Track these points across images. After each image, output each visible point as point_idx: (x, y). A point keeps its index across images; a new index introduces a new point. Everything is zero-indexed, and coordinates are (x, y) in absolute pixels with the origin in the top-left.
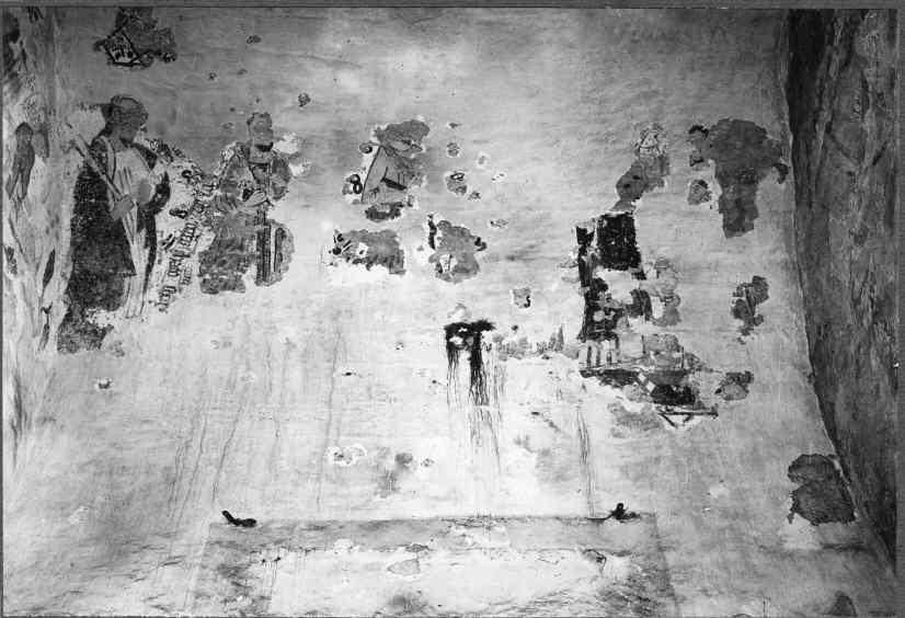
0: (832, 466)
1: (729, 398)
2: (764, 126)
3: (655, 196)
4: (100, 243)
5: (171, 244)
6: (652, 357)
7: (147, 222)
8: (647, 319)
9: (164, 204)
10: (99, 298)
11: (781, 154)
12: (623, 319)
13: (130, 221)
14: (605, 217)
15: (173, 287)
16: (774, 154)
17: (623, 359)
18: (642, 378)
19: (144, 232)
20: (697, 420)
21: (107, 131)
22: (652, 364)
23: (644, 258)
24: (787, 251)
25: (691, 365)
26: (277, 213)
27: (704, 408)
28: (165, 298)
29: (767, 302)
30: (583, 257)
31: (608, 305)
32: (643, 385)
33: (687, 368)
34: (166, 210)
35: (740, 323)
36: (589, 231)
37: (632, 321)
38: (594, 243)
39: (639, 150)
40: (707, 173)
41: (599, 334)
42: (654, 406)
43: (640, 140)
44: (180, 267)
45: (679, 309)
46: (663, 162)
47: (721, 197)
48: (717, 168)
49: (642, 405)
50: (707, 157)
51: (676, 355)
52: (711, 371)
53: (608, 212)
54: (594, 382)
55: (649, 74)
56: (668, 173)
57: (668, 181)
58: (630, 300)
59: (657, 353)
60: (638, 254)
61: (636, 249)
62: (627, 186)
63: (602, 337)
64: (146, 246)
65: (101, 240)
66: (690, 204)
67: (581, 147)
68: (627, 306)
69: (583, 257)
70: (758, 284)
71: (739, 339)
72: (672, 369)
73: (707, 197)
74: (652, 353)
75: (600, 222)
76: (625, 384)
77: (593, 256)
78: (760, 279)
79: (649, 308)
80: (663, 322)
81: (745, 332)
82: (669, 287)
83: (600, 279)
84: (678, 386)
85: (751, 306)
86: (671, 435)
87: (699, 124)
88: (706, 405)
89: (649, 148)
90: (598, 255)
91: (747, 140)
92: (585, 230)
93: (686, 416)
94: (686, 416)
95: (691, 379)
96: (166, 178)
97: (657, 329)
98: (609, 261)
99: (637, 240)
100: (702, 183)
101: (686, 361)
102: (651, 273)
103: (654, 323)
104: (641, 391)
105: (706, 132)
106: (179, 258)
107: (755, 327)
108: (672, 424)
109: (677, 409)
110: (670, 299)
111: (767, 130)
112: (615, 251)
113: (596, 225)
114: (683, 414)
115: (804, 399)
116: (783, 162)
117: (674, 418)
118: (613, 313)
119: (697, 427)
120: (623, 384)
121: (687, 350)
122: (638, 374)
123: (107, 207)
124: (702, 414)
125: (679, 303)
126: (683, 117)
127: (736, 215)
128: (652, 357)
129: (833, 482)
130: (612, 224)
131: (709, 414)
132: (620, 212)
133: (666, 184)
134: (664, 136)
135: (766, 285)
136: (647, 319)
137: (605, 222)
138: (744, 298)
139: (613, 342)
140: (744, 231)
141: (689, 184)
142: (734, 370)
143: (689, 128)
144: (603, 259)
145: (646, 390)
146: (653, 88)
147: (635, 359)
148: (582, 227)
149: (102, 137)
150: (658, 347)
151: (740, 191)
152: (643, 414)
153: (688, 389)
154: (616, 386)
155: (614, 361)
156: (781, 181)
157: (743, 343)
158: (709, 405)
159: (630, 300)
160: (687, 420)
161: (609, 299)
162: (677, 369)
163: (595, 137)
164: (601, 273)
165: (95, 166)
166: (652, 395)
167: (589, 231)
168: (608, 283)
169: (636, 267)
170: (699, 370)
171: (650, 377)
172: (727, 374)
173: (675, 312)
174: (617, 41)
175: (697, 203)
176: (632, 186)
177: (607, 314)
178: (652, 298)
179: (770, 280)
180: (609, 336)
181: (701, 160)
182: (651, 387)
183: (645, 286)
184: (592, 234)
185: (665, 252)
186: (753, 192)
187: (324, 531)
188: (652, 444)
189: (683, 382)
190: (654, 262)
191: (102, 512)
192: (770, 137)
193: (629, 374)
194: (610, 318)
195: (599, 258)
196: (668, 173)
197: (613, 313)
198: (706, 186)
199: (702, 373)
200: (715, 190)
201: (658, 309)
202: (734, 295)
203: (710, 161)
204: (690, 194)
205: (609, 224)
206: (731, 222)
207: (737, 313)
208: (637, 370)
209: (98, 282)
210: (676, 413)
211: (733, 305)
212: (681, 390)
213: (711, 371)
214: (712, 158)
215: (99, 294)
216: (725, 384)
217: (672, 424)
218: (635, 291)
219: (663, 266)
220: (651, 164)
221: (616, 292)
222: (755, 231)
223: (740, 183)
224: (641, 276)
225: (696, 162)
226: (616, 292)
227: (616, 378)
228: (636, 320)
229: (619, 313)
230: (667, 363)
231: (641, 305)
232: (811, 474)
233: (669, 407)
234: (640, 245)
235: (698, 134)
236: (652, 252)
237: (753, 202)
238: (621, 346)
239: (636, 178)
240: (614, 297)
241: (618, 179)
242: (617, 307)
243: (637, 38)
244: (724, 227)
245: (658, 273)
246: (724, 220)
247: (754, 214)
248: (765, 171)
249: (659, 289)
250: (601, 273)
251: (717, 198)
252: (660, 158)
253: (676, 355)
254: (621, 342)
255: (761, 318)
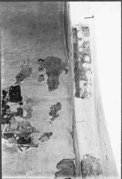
0: (73, 163)
1: (43, 141)
2: (61, 58)
3: (27, 80)
6: (20, 129)
8: (21, 117)
11: (66, 66)
12: (13, 117)
14: (12, 87)
16: (64, 66)
17: (11, 130)
18: (15, 135)
20: (30, 148)
22: (20, 131)
23: (23, 98)
24: (68, 95)
25: (33, 131)
26: (6, 105)
27: (34, 145)
29: (60, 111)
30: (4, 99)
31: (9, 113)
32: (15, 138)
33: (31, 132)
35: (51, 117)
36: (6, 91)
37: (15, 117)
38: (8, 95)
39: (23, 67)
40: (44, 72)
41: (5, 122)
42: (17, 144)
43: (23, 64)
45: (32, 113)
46: (30, 69)
47: (48, 79)
48: (47, 71)
49: (13, 144)
50: (44, 68)
51: (28, 128)
52: (39, 132)
53: (13, 85)
55: (25, 45)
56: (32, 73)
57: (32, 75)
58: (16, 111)
59: (22, 127)
60: (22, 98)
61: (21, 96)
62: (19, 77)
63: (5, 123)
66: (38, 82)
67: (6, 66)
68: (15, 113)
69: (4, 99)
70: (58, 105)
71: (50, 122)
72: (26, 132)
73: (44, 79)
74: (21, 127)
75: (10, 88)
76: (9, 138)
77: (7, 98)
78: (59, 103)
79: (22, 113)
80: (26, 118)
81: (52, 120)
82: (30, 107)
83: (8, 106)
84: (26, 138)
85: (55, 111)
86: (20, 154)
87: (41, 58)
88: (35, 144)
89: (26, 66)
90: (9, 98)
91: (56, 62)
92: (5, 91)
93: (27, 148)
94: (27, 148)
95: (32, 135)
97: (24, 120)
98: (12, 100)
99: (21, 93)
100: (42, 76)
101: (31, 129)
102: (25, 103)
103: (23, 118)
104: (14, 140)
105: (43, 61)
107: (56, 118)
108: (21, 150)
109: (25, 145)
110: (29, 111)
111: (62, 59)
112: (14, 97)
113: (9, 89)
114: (26, 147)
115: (68, 140)
116: (67, 68)
117: (22, 148)
118: (10, 115)
119: (30, 150)
120: (8, 138)
121: (32, 126)
122: (14, 134)
124: (32, 147)
125: (32, 111)
126: (37, 57)
127: (52, 84)
128: (20, 129)
129: (72, 168)
130: (14, 89)
131: (35, 146)
132: (17, 85)
133: (31, 76)
134: (31, 62)
135: (61, 105)
136: (21, 117)
137: (12, 88)
138: (54, 109)
139: (9, 124)
140: (55, 89)
141: (38, 76)
142: (47, 132)
143: (38, 60)
144: (10, 100)
145: (16, 139)
146: (27, 48)
147: (14, 130)
148: (4, 90)
150: (23, 125)
151: (54, 77)
152: (12, 147)
153: (30, 139)
154: (6, 139)
155: (7, 130)
156: (66, 73)
157: (51, 123)
158: (35, 144)
159: (16, 111)
160: (27, 149)
161: (10, 111)
162: (28, 132)
163: (10, 64)
164: (9, 104)
166: (17, 141)
167: (6, 91)
168: (10, 106)
169: (21, 101)
170: (35, 132)
171: (18, 135)
172: (44, 133)
173: (30, 114)
174: (15, 35)
175: (41, 81)
176: (20, 77)
177: (8, 116)
178: (24, 110)
179: (62, 103)
180: (7, 122)
181: (42, 69)
182: (18, 138)
183: (22, 107)
184: (7, 92)
185: (30, 96)
186: (58, 77)
188: (12, 157)
189: (29, 137)
190: (26, 100)
192: (62, 61)
193: (11, 134)
194: (9, 117)
195: (9, 99)
196: (32, 73)
197: (10, 115)
198: (43, 76)
199: (36, 133)
200: (46, 77)
201: (25, 113)
202: (50, 108)
203: (44, 69)
204: (38, 79)
205: (13, 89)
206: (51, 87)
207: (51, 114)
208: (14, 133)
210: (24, 147)
211: (50, 112)
212: (28, 139)
213: (39, 132)
214: (45, 68)
216: (43, 136)
217: (21, 150)
218: (18, 108)
219: (29, 101)
220: (26, 70)
221: (12, 109)
222: (58, 89)
223: (54, 75)
224: (21, 104)
225: (40, 69)
226: (12, 109)
227: (7, 136)
228: (18, 117)
229: (12, 115)
230: (25, 130)
231: (20, 113)
232: (65, 166)
233: (22, 145)
234: (22, 95)
235: (41, 61)
236: (26, 97)
237: (57, 80)
238: (11, 126)
239: (22, 75)
240: (11, 110)
241: (16, 75)
242: (12, 113)
243: (21, 34)
244: (49, 88)
245: (27, 103)
246: (49, 86)
247: (58, 84)
248: (61, 71)
249: (26, 108)
250: (9, 104)
251: (47, 80)
252: (29, 68)
253: (28, 128)
254: (11, 124)
255: (58, 115)
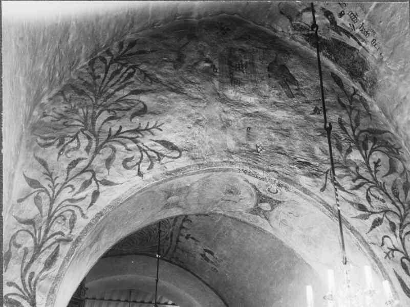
4: (338, 52)
5: (353, 26)
7: (339, 30)
9: (334, 18)
10: (361, 69)
13: (333, 34)
15: (374, 40)
19: (350, 37)
21: (291, 20)
28: (376, 46)
34: (337, 18)
44: (366, 30)
54: (368, 234)
64: (349, 37)
65: (337, 51)
96: (323, 9)
106: (362, 28)
114: (123, 133)
123: (324, 39)
149: (293, 23)
165: (306, 33)
187: (250, 184)
191: (91, 80)
209: (354, 64)
215: (360, 68)
